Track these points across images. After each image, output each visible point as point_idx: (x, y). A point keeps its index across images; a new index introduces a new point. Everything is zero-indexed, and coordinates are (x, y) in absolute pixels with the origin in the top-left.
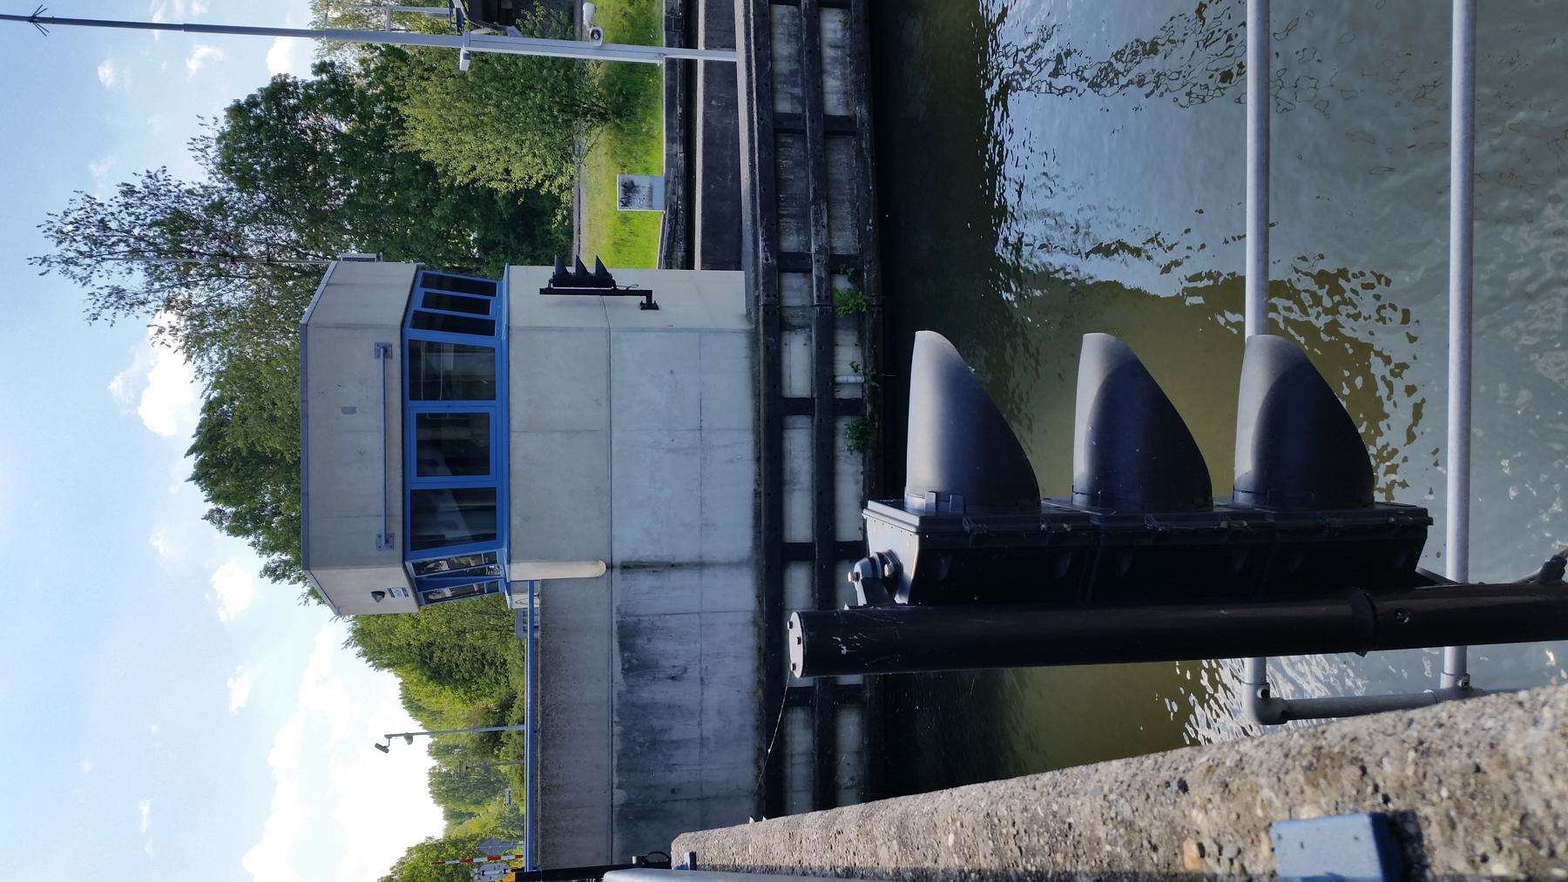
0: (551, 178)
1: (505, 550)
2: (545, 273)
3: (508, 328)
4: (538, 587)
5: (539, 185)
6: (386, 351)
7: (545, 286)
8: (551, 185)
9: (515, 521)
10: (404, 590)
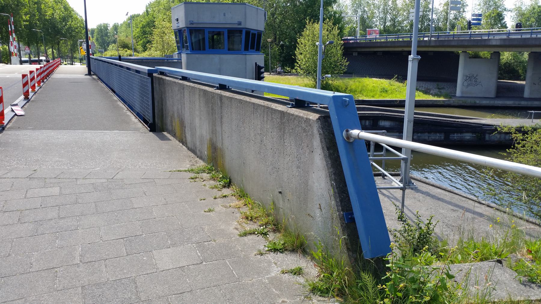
0: (300, 67)
1: (189, 53)
2: (262, 64)
3: (246, 54)
4: (180, 61)
5: (297, 63)
6: (240, 24)
7: (257, 64)
8: (297, 66)
9: (197, 55)
10: (179, 26)
